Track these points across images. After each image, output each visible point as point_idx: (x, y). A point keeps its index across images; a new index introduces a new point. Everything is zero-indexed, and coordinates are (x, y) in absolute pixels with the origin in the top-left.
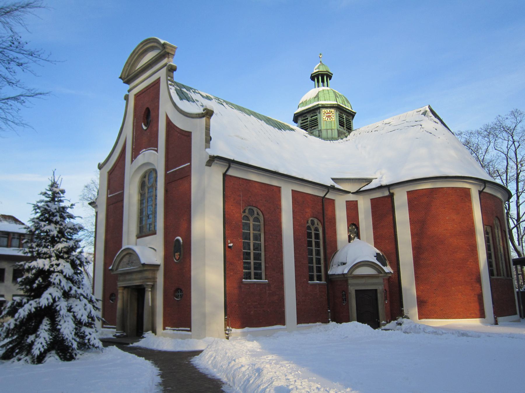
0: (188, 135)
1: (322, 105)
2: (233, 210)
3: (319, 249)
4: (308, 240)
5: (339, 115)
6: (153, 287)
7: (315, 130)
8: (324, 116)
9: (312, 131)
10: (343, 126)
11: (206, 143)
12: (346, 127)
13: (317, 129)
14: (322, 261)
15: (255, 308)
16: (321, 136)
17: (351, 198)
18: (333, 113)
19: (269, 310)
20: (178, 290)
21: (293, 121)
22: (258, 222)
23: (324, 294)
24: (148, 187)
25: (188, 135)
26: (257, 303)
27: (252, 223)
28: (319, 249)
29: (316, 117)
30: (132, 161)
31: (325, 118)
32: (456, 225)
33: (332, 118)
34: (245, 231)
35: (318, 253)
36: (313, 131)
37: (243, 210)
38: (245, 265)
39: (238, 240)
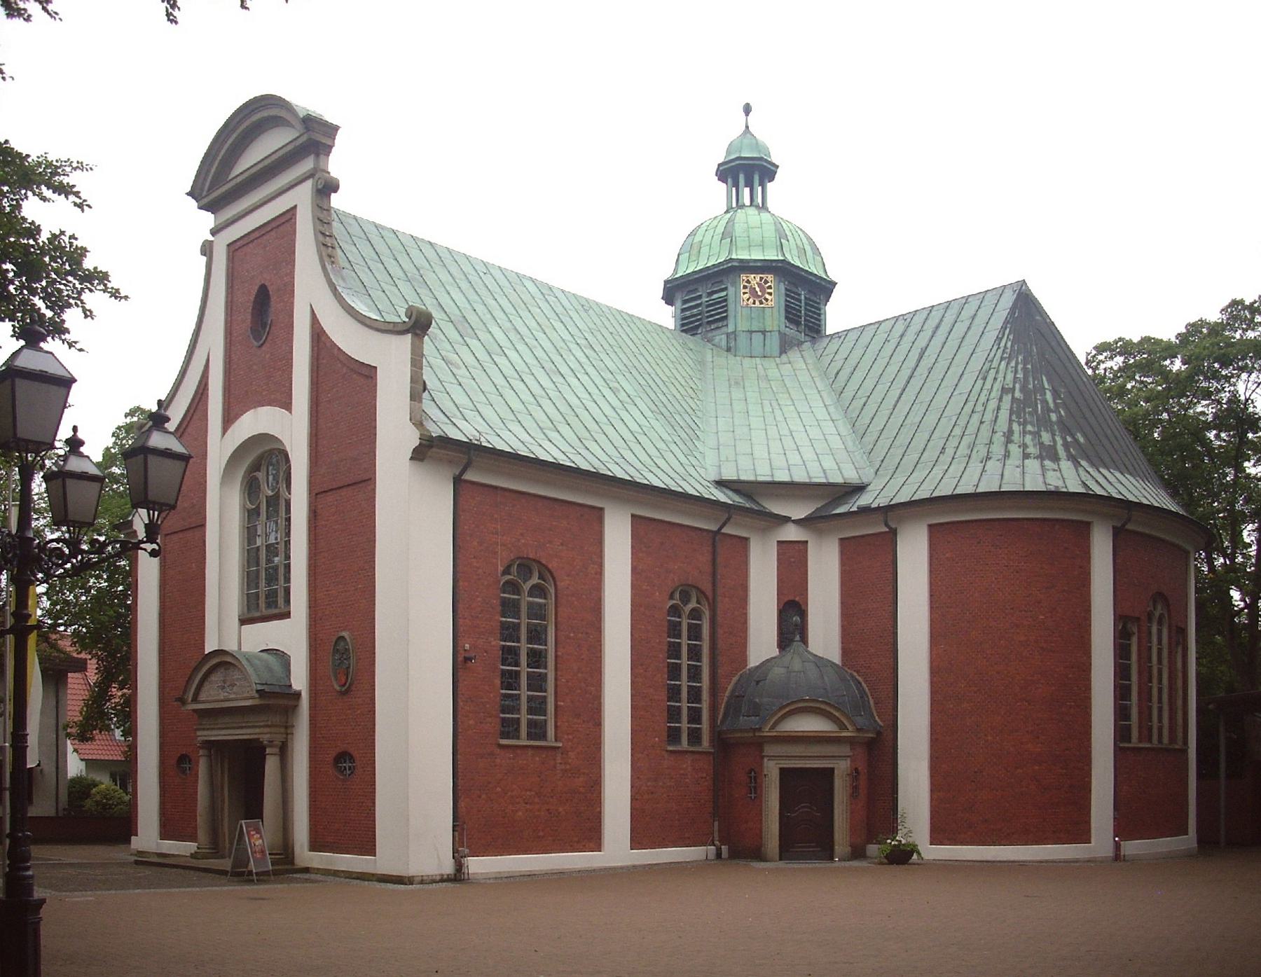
0: (367, 373)
1: (741, 261)
2: (478, 568)
3: (699, 664)
4: (669, 642)
5: (786, 289)
6: (284, 751)
7: (718, 332)
8: (744, 293)
9: (710, 335)
10: (797, 323)
11: (411, 400)
12: (805, 325)
13: (724, 329)
14: (705, 696)
15: (526, 803)
16: (732, 350)
17: (791, 533)
18: (769, 284)
19: (561, 809)
20: (343, 756)
21: (663, 298)
22: (541, 598)
23: (704, 775)
24: (267, 497)
25: (367, 373)
26: (533, 793)
27: (526, 600)
28: (699, 664)
29: (723, 294)
30: (225, 430)
31: (748, 300)
32: (1044, 615)
33: (767, 300)
34: (508, 620)
35: (695, 674)
36: (714, 333)
37: (502, 569)
38: (507, 703)
39: (490, 643)
